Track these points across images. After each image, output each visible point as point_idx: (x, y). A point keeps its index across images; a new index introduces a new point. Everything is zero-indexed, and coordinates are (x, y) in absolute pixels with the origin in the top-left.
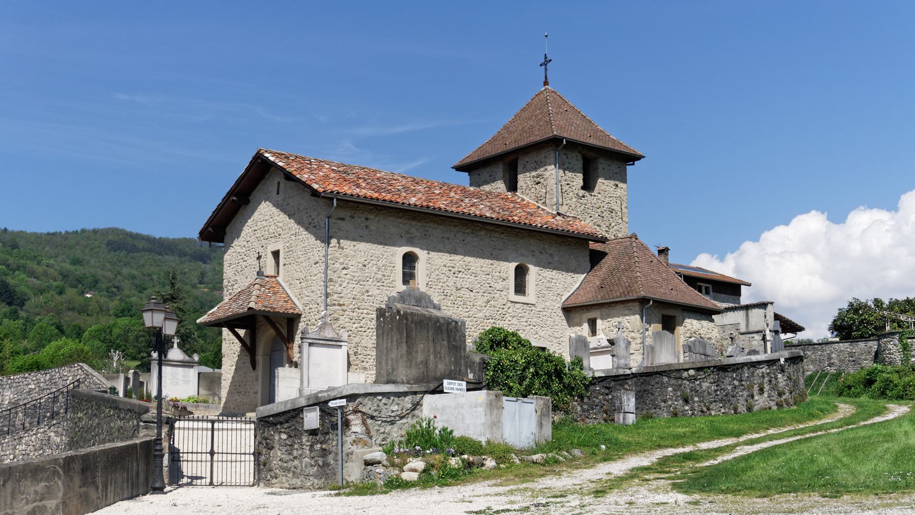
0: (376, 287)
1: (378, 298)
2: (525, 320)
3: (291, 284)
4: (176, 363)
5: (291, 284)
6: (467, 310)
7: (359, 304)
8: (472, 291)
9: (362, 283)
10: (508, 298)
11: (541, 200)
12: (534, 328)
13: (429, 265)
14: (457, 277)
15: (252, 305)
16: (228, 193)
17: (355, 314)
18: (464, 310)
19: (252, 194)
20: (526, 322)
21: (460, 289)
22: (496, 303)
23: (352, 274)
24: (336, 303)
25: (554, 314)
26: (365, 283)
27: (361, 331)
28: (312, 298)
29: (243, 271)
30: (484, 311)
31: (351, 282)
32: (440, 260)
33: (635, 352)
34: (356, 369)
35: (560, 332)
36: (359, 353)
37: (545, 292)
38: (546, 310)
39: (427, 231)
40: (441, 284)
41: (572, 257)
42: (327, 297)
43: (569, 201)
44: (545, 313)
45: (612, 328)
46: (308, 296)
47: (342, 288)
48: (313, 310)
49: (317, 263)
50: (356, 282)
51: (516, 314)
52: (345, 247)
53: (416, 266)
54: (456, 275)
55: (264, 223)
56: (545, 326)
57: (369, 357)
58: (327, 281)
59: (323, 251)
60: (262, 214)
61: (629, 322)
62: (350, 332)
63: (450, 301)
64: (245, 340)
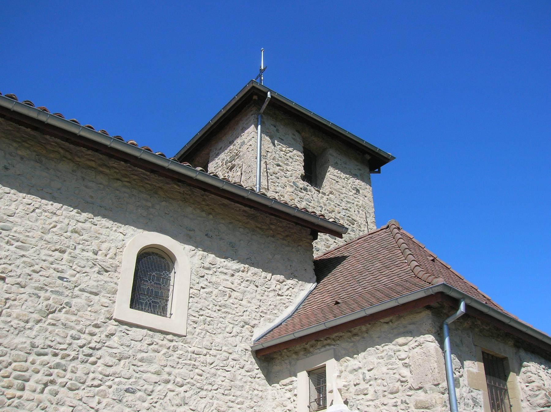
2: (154, 367)
12: (178, 389)
20: (158, 373)
22: (74, 318)
25: (233, 363)
30: (33, 333)
38: (212, 352)
45: (363, 385)
56: (210, 387)
61: (406, 365)
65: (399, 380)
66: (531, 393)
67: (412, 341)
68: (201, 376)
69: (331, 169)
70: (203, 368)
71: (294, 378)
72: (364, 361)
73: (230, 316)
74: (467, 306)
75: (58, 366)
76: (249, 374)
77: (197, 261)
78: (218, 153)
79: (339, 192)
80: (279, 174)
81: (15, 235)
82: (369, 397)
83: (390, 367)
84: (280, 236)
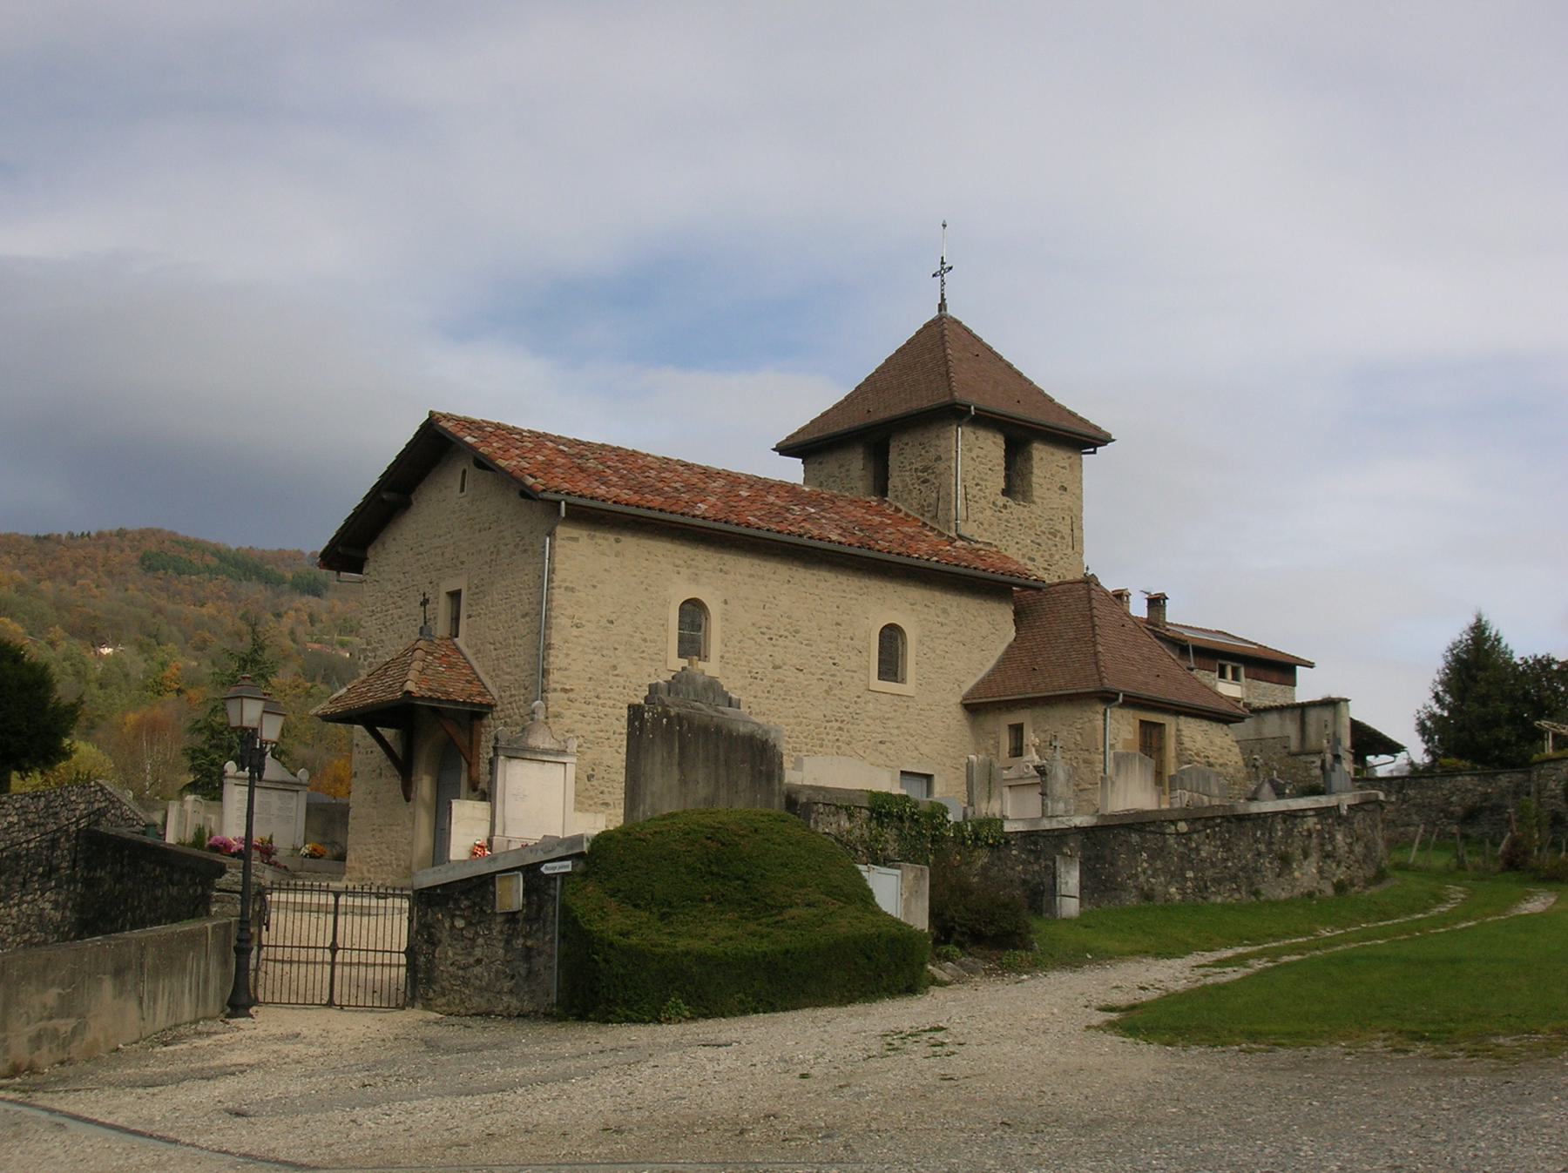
5: (479, 651)
11: (929, 511)
15: (410, 686)
20: (898, 728)
21: (780, 667)
28: (517, 677)
44: (932, 714)
46: (508, 673)
49: (527, 614)
75: (840, 729)
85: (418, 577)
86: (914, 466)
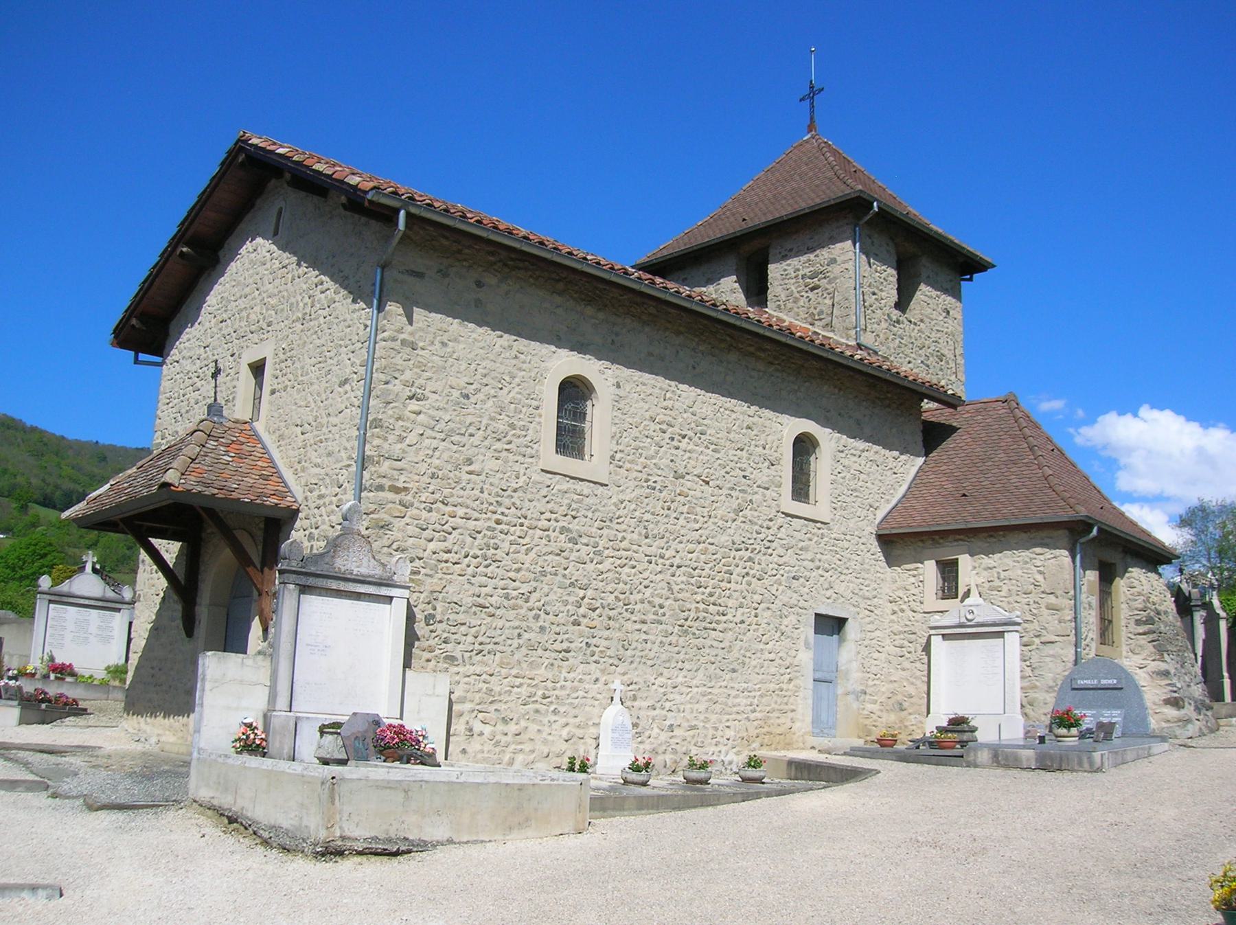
0: (489, 454)
1: (495, 481)
2: (809, 556)
3: (281, 437)
4: (87, 602)
5: (281, 437)
6: (697, 526)
7: (447, 491)
8: (708, 483)
9: (456, 438)
10: (778, 506)
11: (821, 320)
13: (618, 414)
14: (677, 448)
15: (171, 477)
16: (173, 239)
17: (434, 516)
18: (689, 526)
19: (226, 245)
20: (812, 561)
21: (683, 477)
22: (756, 514)
23: (431, 412)
24: (386, 483)
26: (464, 440)
27: (446, 562)
28: (328, 470)
29: (191, 413)
30: (731, 531)
31: (429, 432)
32: (642, 404)
33: (1057, 639)
34: (428, 660)
35: (874, 585)
36: (438, 618)
37: (848, 500)
39: (617, 334)
40: (642, 460)
41: (894, 430)
42: (363, 468)
43: (875, 326)
44: (846, 544)
45: (997, 583)
46: (318, 466)
47: (403, 446)
48: (327, 500)
49: (346, 381)
50: (443, 436)
51: (794, 542)
52: (421, 344)
53: (589, 411)
54: (675, 443)
55: (242, 303)
57: (463, 629)
58: (367, 424)
59: (364, 351)
60: (239, 284)
61: (1040, 572)
62: (417, 563)
63: (661, 503)
64: (176, 572)
65: (1033, 584)
66: (1131, 597)
67: (1049, 553)
68: (840, 560)
69: (923, 287)
70: (842, 554)
71: (919, 565)
72: (1000, 562)
73: (860, 499)
74: (1100, 530)
75: (750, 559)
76: (874, 557)
77: (833, 444)
78: (786, 255)
79: (930, 318)
80: (874, 306)
81: (710, 438)
82: (1002, 594)
83: (1025, 571)
84: (895, 406)
85: (220, 350)
86: (801, 273)
